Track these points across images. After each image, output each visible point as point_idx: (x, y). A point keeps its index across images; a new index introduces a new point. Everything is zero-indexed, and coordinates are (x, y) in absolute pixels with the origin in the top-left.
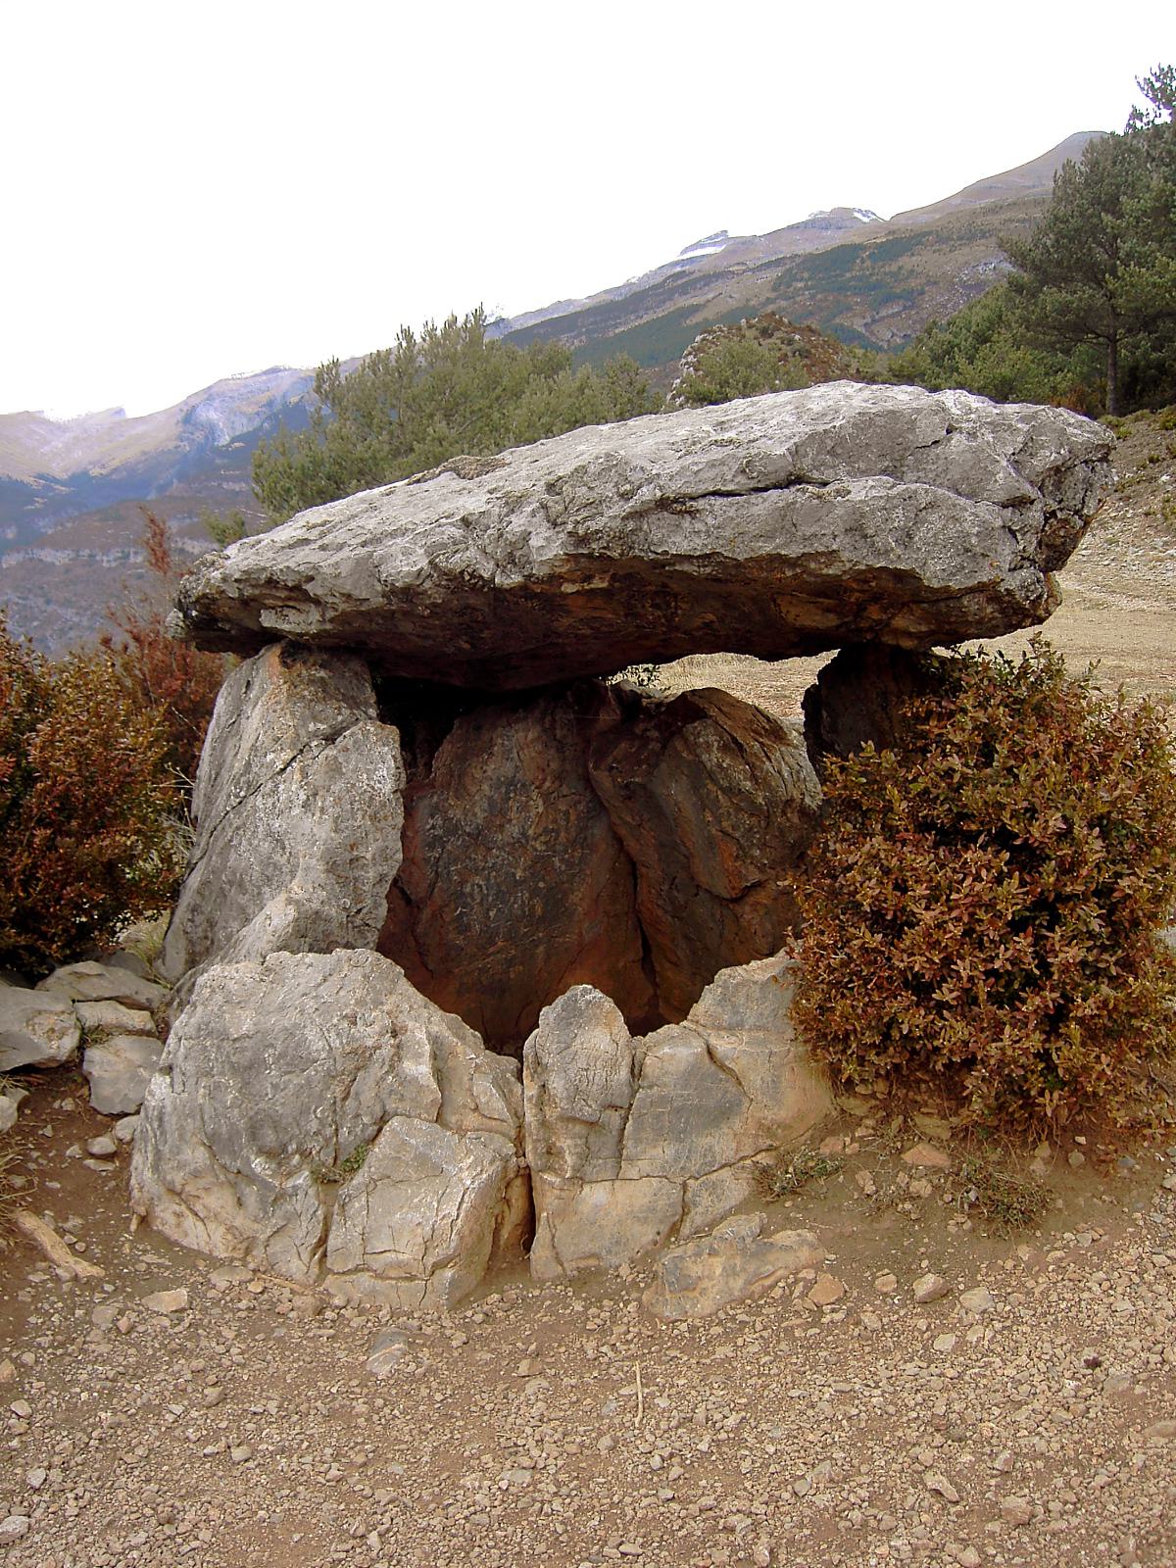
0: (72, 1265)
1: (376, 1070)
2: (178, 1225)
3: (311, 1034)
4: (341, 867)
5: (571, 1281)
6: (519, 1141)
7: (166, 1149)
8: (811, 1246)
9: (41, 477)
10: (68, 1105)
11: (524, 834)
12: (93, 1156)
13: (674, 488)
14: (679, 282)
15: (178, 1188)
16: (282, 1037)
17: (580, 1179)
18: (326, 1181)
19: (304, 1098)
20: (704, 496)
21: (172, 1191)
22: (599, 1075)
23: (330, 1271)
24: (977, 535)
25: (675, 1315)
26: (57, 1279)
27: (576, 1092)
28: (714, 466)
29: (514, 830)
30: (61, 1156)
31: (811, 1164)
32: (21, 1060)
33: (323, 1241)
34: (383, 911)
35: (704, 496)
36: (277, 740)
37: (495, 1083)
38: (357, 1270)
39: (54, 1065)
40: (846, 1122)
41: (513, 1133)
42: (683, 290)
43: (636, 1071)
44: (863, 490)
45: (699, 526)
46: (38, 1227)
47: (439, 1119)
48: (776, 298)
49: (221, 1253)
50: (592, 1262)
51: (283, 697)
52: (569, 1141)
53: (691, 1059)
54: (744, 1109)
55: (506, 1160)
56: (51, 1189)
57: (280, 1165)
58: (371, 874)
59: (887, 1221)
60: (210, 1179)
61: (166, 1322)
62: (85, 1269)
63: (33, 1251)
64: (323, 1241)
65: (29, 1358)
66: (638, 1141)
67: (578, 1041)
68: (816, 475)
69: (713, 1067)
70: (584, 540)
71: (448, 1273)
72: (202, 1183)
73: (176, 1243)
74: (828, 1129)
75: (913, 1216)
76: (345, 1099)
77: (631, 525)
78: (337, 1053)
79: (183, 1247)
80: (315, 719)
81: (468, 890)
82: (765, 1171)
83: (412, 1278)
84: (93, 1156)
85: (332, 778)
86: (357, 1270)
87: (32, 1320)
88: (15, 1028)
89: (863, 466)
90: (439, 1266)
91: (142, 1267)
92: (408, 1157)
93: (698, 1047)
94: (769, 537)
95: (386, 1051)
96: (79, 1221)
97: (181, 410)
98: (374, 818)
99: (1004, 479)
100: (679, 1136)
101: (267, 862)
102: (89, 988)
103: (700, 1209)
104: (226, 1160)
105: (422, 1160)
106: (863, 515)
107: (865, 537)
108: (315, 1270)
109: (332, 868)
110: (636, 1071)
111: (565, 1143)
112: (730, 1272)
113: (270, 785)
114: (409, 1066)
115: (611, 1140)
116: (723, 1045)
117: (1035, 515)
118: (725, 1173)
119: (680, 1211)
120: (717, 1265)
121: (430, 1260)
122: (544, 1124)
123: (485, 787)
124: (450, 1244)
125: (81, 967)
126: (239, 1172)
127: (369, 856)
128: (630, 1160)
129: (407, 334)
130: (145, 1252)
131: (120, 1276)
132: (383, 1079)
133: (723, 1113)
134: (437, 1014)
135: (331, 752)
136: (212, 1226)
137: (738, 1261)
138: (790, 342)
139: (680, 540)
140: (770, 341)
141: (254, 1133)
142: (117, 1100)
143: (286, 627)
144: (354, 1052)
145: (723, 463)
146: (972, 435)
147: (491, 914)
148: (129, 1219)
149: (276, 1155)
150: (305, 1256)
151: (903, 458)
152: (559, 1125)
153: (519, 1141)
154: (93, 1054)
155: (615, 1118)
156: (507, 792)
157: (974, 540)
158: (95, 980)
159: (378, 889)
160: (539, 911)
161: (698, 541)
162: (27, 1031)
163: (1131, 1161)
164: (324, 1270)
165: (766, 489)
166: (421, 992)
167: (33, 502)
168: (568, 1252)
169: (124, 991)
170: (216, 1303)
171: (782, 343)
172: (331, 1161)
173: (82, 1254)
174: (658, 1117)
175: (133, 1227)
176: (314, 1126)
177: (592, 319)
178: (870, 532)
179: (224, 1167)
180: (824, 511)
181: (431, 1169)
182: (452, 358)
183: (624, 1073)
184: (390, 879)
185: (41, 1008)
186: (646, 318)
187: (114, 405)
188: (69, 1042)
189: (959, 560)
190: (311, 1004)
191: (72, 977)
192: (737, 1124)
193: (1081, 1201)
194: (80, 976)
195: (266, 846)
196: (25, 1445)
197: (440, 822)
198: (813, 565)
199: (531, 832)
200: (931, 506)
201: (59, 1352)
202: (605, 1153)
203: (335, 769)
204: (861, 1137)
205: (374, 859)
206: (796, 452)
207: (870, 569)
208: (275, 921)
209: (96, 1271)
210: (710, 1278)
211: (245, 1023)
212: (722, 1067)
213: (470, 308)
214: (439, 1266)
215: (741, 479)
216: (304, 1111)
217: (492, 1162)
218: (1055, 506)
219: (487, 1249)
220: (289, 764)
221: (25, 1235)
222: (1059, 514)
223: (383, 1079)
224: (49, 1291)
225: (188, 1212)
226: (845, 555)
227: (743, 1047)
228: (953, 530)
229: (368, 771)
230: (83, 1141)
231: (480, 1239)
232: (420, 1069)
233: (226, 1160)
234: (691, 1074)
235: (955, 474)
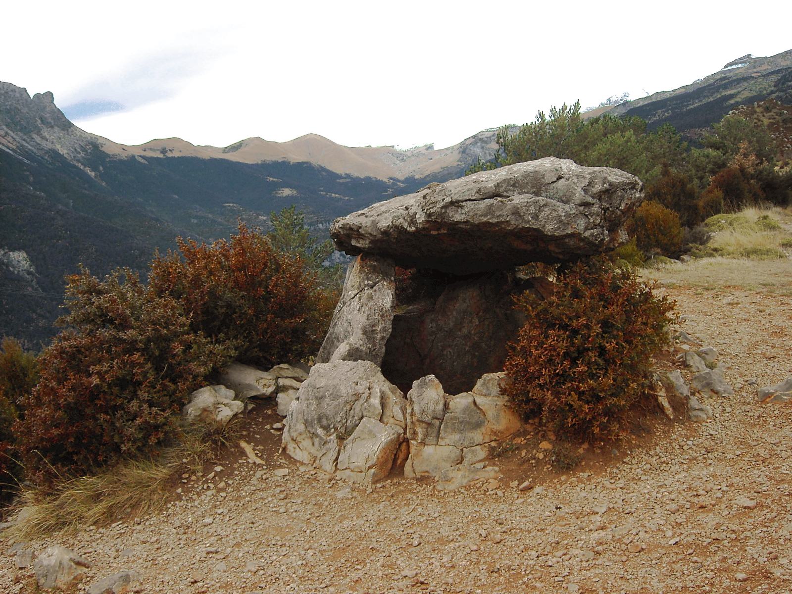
0: (253, 458)
1: (361, 401)
2: (294, 452)
3: (342, 388)
4: (369, 332)
5: (417, 480)
6: (405, 429)
7: (292, 425)
8: (496, 472)
9: (391, 178)
10: (269, 412)
11: (470, 333)
12: (273, 429)
13: (455, 198)
14: (724, 82)
15: (295, 438)
16: (332, 387)
17: (423, 443)
18: (341, 438)
19: (337, 409)
20: (466, 201)
21: (293, 439)
22: (432, 406)
23: (338, 469)
24: (564, 216)
25: (441, 489)
26: (248, 463)
27: (423, 412)
28: (469, 190)
29: (465, 331)
30: (263, 428)
31: (508, 446)
32: (253, 394)
33: (337, 459)
34: (384, 350)
35: (466, 201)
36: (353, 286)
37: (401, 408)
38: (346, 469)
39: (264, 397)
40: (525, 433)
41: (404, 426)
42: (725, 87)
43: (446, 406)
44: (518, 199)
45: (463, 211)
46: (247, 448)
47: (381, 420)
48: (776, 91)
49: (306, 462)
50: (426, 474)
51: (358, 271)
52: (420, 429)
53: (466, 404)
54: (486, 424)
55: (399, 435)
56: (256, 438)
57: (327, 432)
58: (379, 336)
59: (525, 466)
60: (305, 435)
61: (279, 478)
62: (258, 461)
63: (243, 453)
64: (337, 459)
65: (230, 482)
66: (446, 432)
67: (425, 393)
68: (505, 194)
69: (475, 408)
70: (430, 215)
71: (373, 470)
72: (302, 437)
73: (293, 458)
74: (518, 434)
75: (534, 465)
76: (350, 410)
77: (443, 211)
78: (350, 394)
79: (294, 459)
80: (368, 279)
81: (445, 353)
82: (493, 448)
83: (361, 472)
84: (273, 429)
85: (369, 301)
86: (346, 469)
87: (235, 472)
88: (252, 383)
89: (525, 190)
90: (370, 468)
91: (278, 463)
92: (366, 430)
93: (470, 400)
94: (485, 215)
95: (366, 395)
96: (262, 448)
97: (461, 147)
98: (382, 316)
99: (579, 195)
100: (461, 431)
101: (346, 331)
102: (284, 373)
103: (467, 459)
104: (309, 429)
105: (370, 432)
106: (518, 208)
107: (521, 216)
108: (334, 469)
109: (365, 333)
110: (446, 406)
111: (419, 430)
112: (464, 477)
113: (349, 302)
114: (372, 400)
115: (435, 430)
116: (480, 400)
117: (595, 209)
118: (478, 447)
119: (460, 459)
120: (460, 474)
121: (367, 466)
122: (412, 422)
123: (454, 313)
124: (373, 460)
125: (282, 366)
126: (313, 433)
127: (379, 330)
128: (442, 438)
129: (541, 115)
130: (281, 459)
131: (270, 465)
132: (363, 404)
133: (478, 425)
134: (388, 383)
135: (370, 291)
136: (304, 452)
137: (467, 474)
138: (781, 114)
139: (458, 216)
140: (770, 114)
141: (319, 420)
142: (285, 411)
143: (359, 245)
144: (355, 394)
145: (472, 189)
146: (568, 180)
147: (455, 364)
148: (279, 449)
149: (326, 428)
150: (331, 463)
151: (541, 188)
152: (417, 423)
153: (405, 429)
154: (280, 395)
155: (437, 422)
156: (464, 315)
157: (563, 218)
158: (286, 370)
159: (381, 342)
160: (475, 364)
161: (463, 216)
162: (256, 384)
163: (617, 452)
164: (337, 469)
165: (485, 199)
166: (384, 376)
167: (387, 191)
168: (417, 469)
169: (296, 375)
170: (298, 475)
171: (777, 115)
172: (344, 432)
173: (260, 457)
174: (453, 424)
175: (280, 452)
176: (339, 419)
177: (674, 102)
178: (522, 214)
179: (309, 431)
180: (503, 207)
181: (372, 435)
182: (562, 128)
183: (441, 406)
184: (386, 339)
185: (262, 377)
186: (704, 101)
187: (429, 143)
188: (271, 389)
189: (558, 225)
190: (343, 377)
191: (278, 369)
192: (483, 429)
193: (592, 463)
194: (281, 369)
195: (346, 325)
196: (221, 504)
197: (435, 325)
198: (503, 226)
199: (472, 332)
200: (545, 205)
201: (241, 482)
202: (434, 435)
203: (371, 298)
204: (528, 439)
205: (380, 330)
206: (498, 186)
207: (524, 228)
208: (341, 350)
209: (263, 462)
210: (456, 478)
211: (322, 383)
212: (479, 408)
213: (570, 103)
214: (370, 468)
215: (477, 195)
216: (336, 413)
217: (393, 434)
218: (608, 206)
219: (390, 465)
220: (356, 295)
221: (241, 448)
222: (610, 209)
223: (363, 404)
224: (245, 466)
225: (297, 447)
226: (513, 222)
227: (487, 402)
228: (554, 214)
229: (382, 299)
230: (272, 424)
231: (386, 461)
232: (376, 401)
233: (309, 429)
234: (466, 410)
235: (561, 194)
